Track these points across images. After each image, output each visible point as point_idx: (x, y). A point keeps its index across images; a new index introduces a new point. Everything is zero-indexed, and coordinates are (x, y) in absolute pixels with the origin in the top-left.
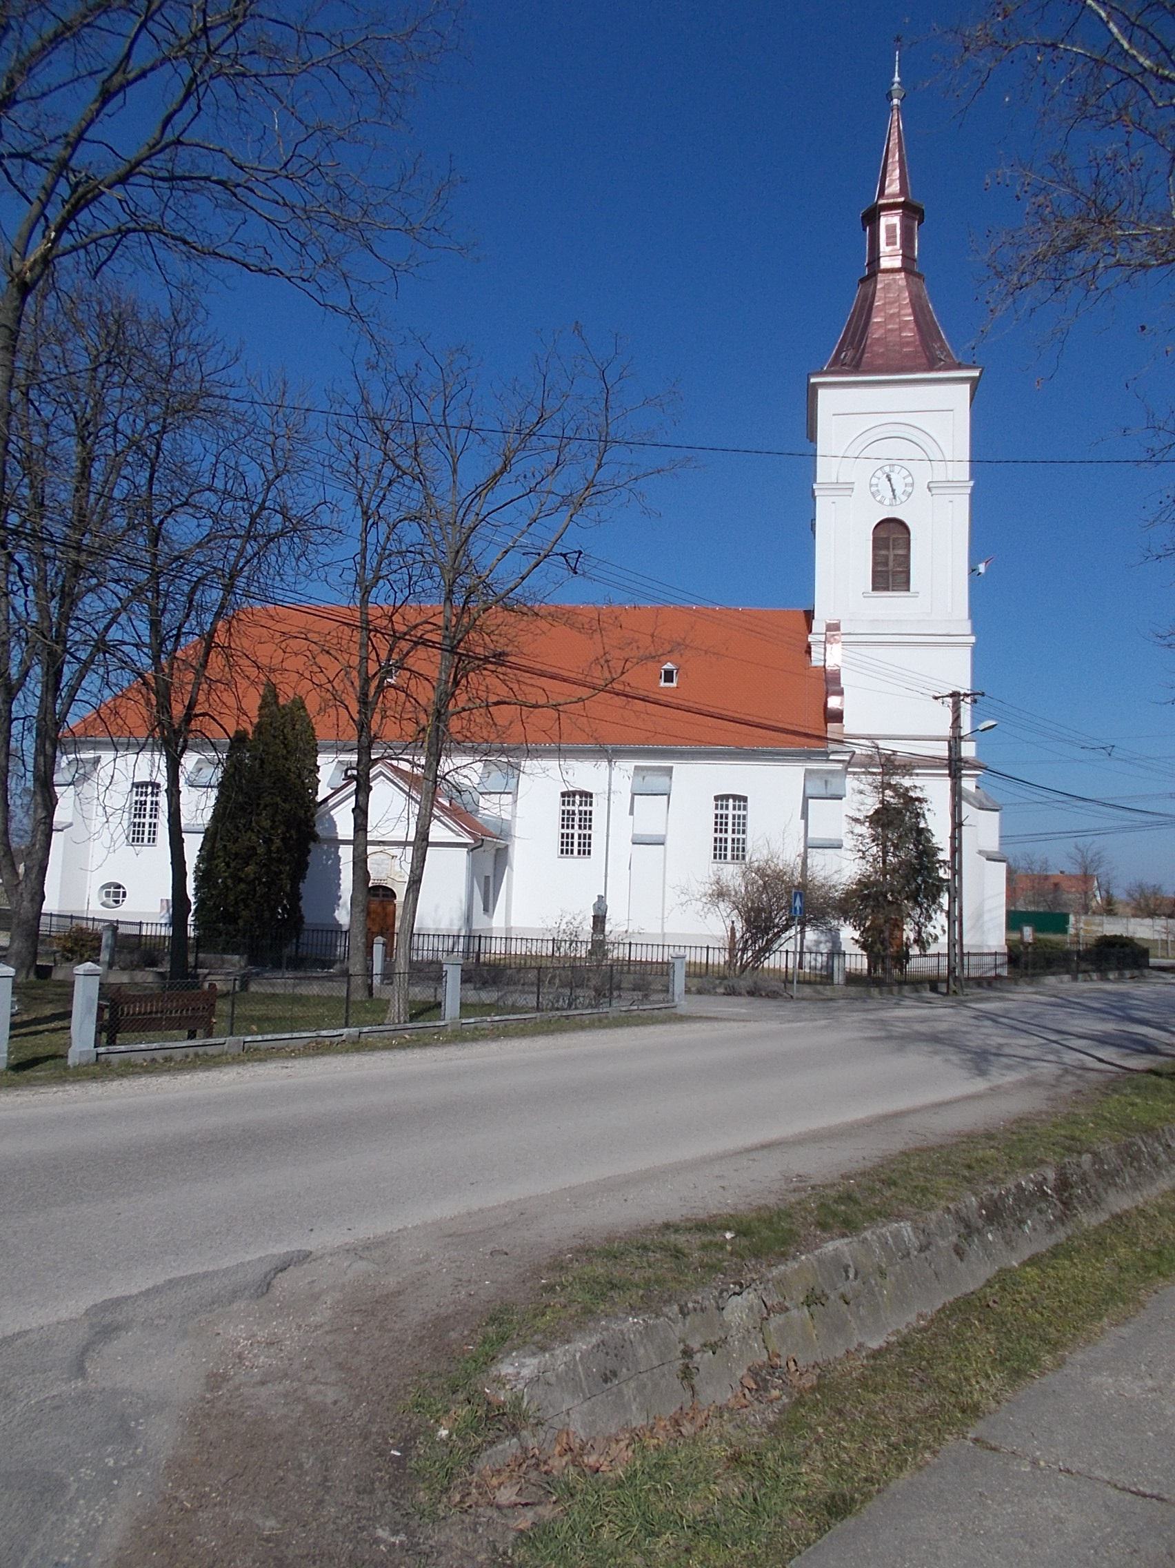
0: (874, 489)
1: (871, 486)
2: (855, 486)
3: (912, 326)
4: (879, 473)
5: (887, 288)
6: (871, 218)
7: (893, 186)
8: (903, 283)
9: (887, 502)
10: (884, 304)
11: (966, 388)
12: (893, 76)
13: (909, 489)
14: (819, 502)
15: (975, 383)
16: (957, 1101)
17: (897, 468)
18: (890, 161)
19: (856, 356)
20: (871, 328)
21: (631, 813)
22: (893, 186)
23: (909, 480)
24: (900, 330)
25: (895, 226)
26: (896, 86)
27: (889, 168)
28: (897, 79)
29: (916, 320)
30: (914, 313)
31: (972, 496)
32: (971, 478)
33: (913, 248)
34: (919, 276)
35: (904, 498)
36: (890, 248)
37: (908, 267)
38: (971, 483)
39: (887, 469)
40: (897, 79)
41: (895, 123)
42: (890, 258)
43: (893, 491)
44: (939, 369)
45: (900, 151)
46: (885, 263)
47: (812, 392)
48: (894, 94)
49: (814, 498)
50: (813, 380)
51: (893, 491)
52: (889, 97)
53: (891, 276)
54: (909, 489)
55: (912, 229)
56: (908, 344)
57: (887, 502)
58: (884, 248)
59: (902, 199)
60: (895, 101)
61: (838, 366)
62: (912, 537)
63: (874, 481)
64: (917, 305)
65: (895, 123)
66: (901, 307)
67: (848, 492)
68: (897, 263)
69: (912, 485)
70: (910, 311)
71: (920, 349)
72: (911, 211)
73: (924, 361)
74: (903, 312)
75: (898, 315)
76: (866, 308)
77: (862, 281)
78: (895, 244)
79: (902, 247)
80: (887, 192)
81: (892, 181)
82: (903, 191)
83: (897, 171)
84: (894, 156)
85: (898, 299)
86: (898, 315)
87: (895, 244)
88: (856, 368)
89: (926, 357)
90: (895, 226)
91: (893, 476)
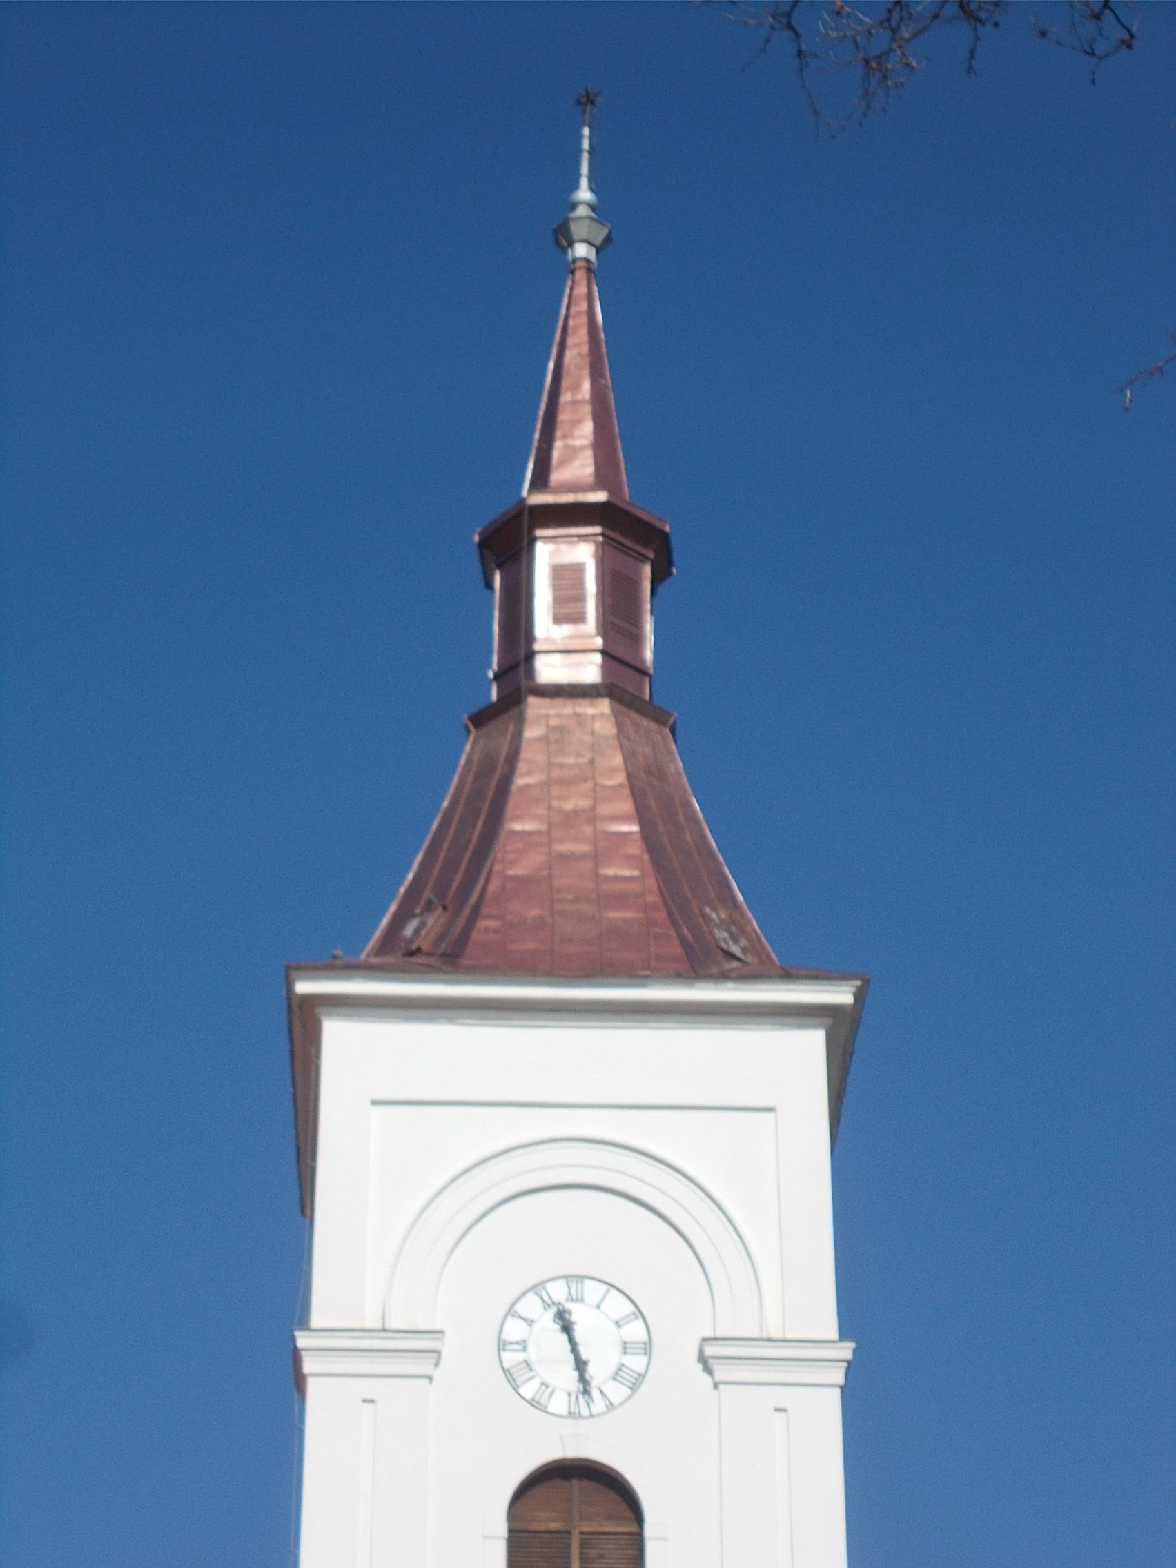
0: (510, 1358)
1: (502, 1345)
2: (448, 1347)
3: (636, 848)
4: (531, 1306)
5: (557, 737)
6: (507, 544)
7: (575, 468)
8: (606, 728)
9: (559, 1404)
10: (547, 784)
11: (811, 1045)
12: (576, 186)
13: (636, 1363)
14: (316, 1391)
15: (845, 1036)
16: (611, 1533)
17: (592, 1291)
18: (566, 397)
19: (457, 923)
20: (502, 849)
21: (374, 1103)
22: (575, 468)
23: (635, 1331)
24: (597, 857)
25: (578, 569)
26: (582, 211)
27: (563, 417)
28: (584, 194)
29: (648, 836)
30: (641, 814)
31: (848, 1393)
32: (845, 1333)
33: (636, 639)
34: (657, 714)
35: (617, 1392)
36: (566, 629)
37: (622, 682)
38: (846, 1351)
39: (558, 1291)
40: (584, 194)
41: (581, 308)
42: (566, 651)
43: (580, 1365)
44: (724, 977)
45: (596, 374)
46: (548, 670)
47: (302, 1025)
48: (577, 230)
49: (299, 1382)
50: (304, 987)
51: (580, 1365)
52: (563, 237)
53: (568, 708)
54: (636, 1363)
55: (635, 584)
56: (620, 900)
57: (559, 1404)
58: (544, 626)
59: (600, 497)
60: (581, 250)
61: (399, 955)
62: (649, 1530)
63: (515, 1330)
64: (646, 791)
65: (581, 308)
66: (597, 795)
67: (425, 1366)
68: (589, 671)
69: (647, 1348)
70: (627, 806)
71: (662, 915)
72: (629, 532)
73: (676, 949)
74: (605, 809)
75: (592, 816)
76: (491, 794)
77: (482, 718)
78: (579, 618)
79: (605, 628)
80: (557, 476)
81: (572, 453)
82: (603, 477)
83: (588, 427)
84: (576, 387)
85: (589, 772)
86: (592, 816)
87: (579, 618)
88: (451, 957)
89: (679, 932)
90: (578, 569)
91: (578, 1315)
